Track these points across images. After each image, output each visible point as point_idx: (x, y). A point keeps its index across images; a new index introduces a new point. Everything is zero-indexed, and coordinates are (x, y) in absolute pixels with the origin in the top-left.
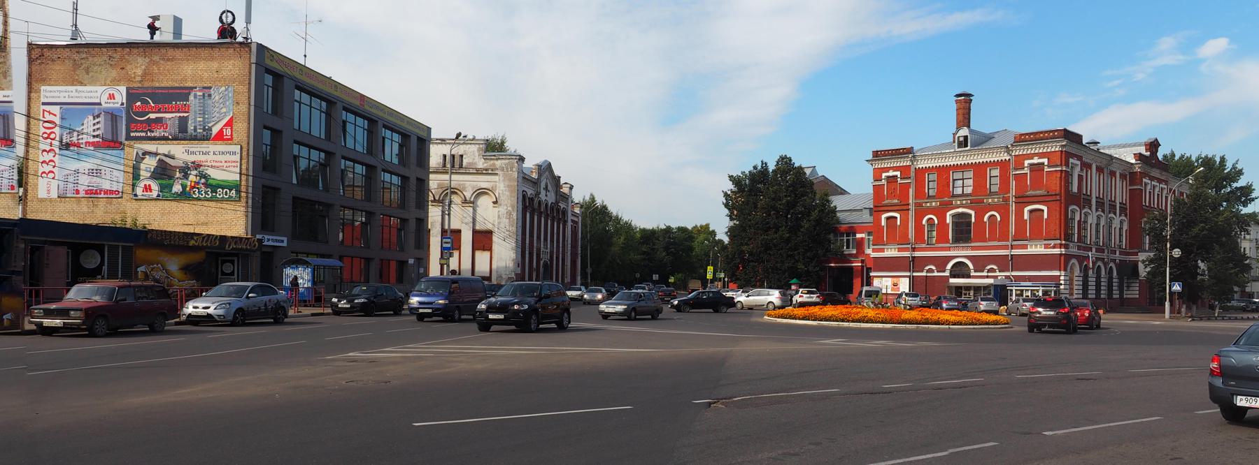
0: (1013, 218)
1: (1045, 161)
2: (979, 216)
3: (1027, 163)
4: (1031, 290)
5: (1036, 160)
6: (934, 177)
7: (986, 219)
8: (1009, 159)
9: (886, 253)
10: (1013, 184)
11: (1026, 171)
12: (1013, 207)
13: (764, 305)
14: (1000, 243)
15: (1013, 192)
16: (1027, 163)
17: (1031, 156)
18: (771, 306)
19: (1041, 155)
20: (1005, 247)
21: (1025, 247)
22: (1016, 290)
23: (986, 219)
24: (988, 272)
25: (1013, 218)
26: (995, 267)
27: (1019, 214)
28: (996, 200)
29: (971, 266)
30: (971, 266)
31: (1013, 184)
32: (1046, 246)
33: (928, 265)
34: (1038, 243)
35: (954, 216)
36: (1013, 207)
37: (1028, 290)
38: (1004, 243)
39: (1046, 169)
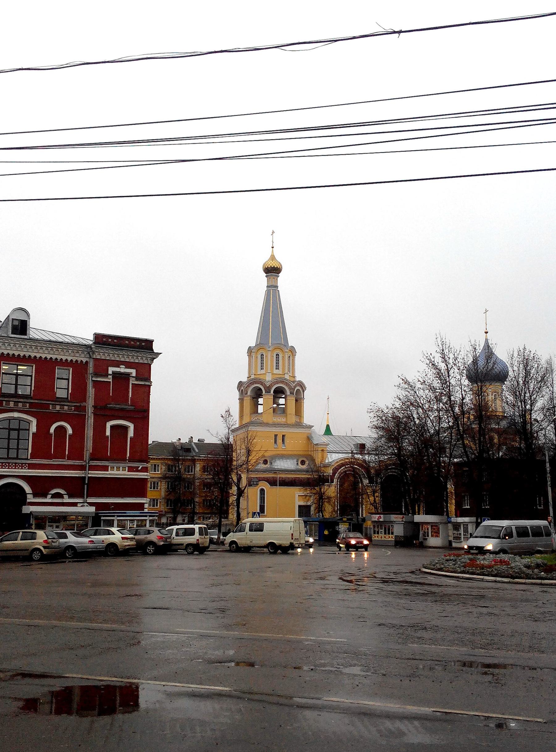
0: (89, 432)
1: (133, 372)
2: (43, 427)
3: (111, 370)
4: (138, 520)
5: (122, 369)
6: (69, 373)
7: (52, 430)
8: (87, 362)
9: (110, 472)
10: (91, 391)
11: (110, 379)
12: (90, 421)
13: (182, 544)
14: (71, 462)
15: (90, 402)
16: (111, 370)
17: (117, 364)
18: (36, 556)
19: (129, 365)
20: (82, 468)
21: (105, 468)
22: (118, 520)
23: (52, 430)
24: (52, 498)
25: (89, 432)
26: (62, 492)
27: (99, 429)
28: (66, 408)
29: (27, 489)
30: (27, 489)
31: (91, 391)
32: (131, 469)
33: (53, 489)
34: (121, 465)
35: (112, 427)
36: (90, 421)
37: (134, 520)
38: (77, 463)
39: (132, 381)
